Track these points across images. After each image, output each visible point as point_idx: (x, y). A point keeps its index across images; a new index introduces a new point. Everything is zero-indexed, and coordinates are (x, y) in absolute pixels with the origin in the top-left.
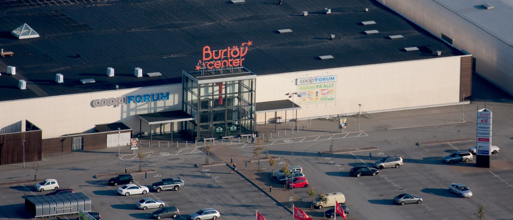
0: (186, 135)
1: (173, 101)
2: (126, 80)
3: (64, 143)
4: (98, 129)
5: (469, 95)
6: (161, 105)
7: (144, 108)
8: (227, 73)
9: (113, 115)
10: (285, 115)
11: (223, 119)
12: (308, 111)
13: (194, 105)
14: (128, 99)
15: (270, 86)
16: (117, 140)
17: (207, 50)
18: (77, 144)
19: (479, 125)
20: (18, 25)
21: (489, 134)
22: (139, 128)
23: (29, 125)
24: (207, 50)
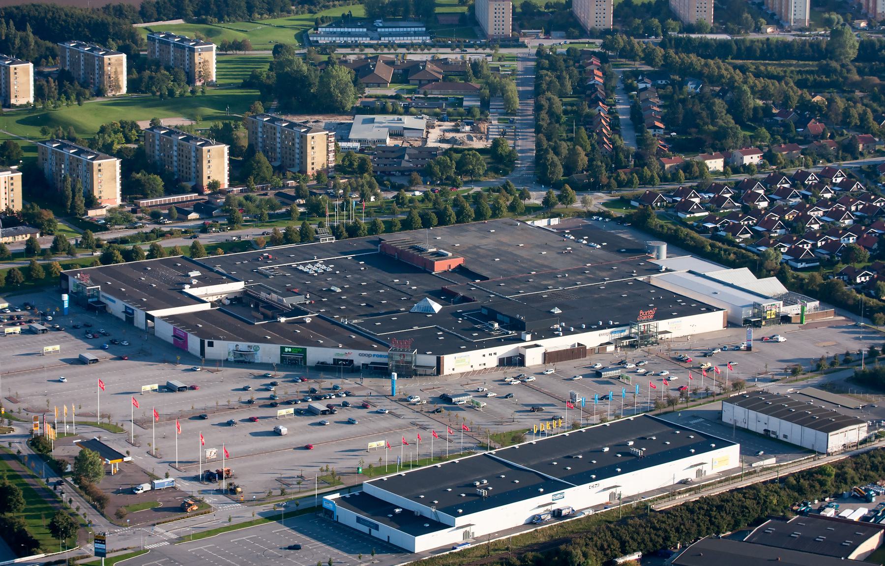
0: (632, 346)
1: (626, 333)
2: (606, 326)
3: (592, 350)
4: (601, 345)
5: (724, 420)
6: (623, 334)
7: (617, 336)
8: (648, 321)
9: (606, 339)
10: (667, 336)
11: (645, 338)
12: (676, 334)
13: (636, 334)
14: (612, 333)
15: (663, 325)
16: (610, 348)
17: (641, 312)
18: (597, 351)
19: (330, 174)
20: (554, 308)
21: (218, 62)
22: (616, 342)
23: (579, 344)
24: (641, 312)
